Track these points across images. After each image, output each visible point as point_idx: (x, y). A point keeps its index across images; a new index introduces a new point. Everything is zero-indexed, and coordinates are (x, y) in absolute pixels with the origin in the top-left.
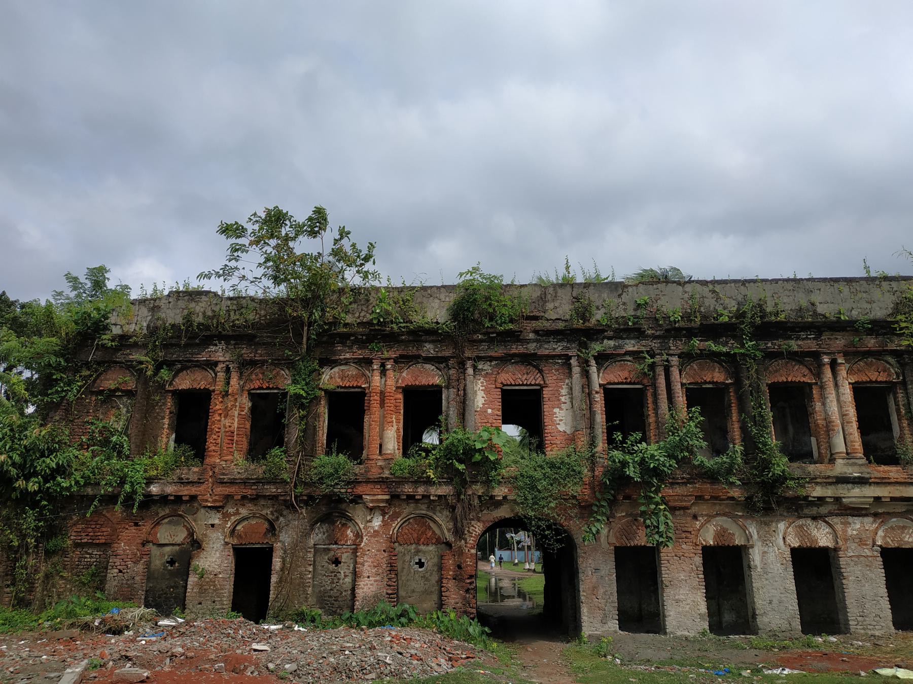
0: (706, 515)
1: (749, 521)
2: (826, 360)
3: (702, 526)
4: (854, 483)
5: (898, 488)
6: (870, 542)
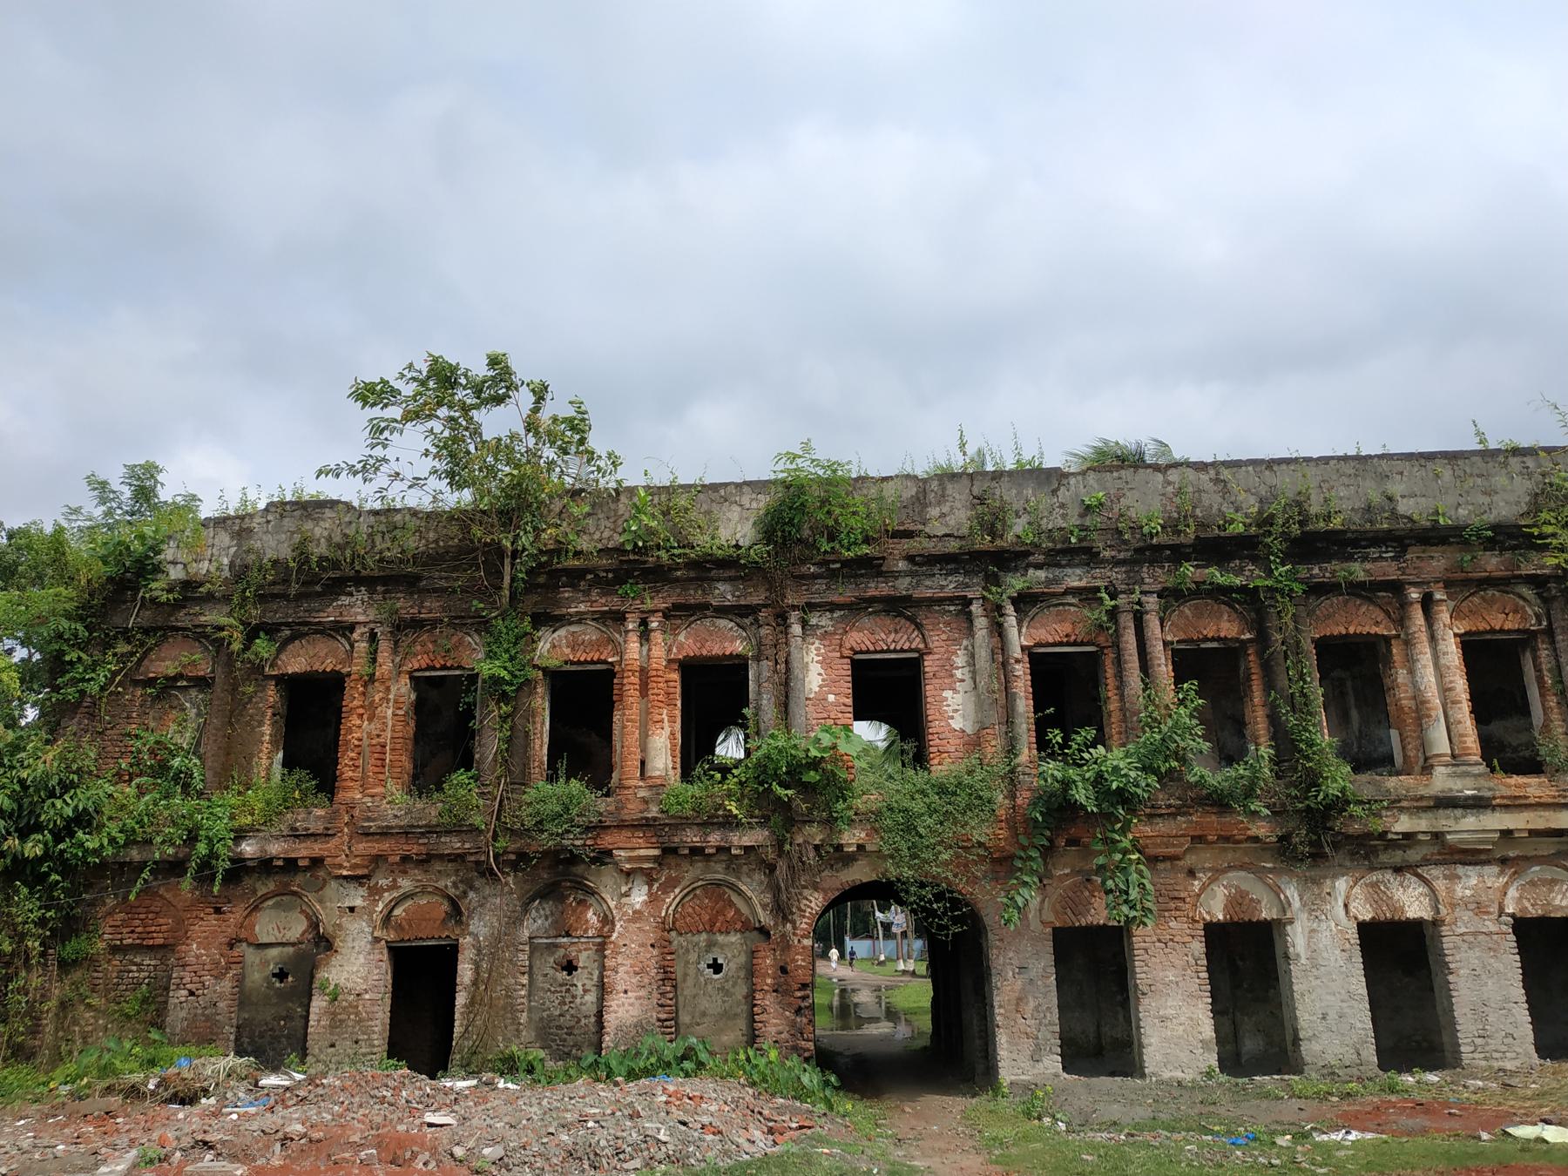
0: (1210, 869)
1: (1285, 878)
2: (1414, 594)
3: (1203, 888)
4: (1465, 807)
5: (1542, 813)
6: (1494, 909)
